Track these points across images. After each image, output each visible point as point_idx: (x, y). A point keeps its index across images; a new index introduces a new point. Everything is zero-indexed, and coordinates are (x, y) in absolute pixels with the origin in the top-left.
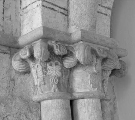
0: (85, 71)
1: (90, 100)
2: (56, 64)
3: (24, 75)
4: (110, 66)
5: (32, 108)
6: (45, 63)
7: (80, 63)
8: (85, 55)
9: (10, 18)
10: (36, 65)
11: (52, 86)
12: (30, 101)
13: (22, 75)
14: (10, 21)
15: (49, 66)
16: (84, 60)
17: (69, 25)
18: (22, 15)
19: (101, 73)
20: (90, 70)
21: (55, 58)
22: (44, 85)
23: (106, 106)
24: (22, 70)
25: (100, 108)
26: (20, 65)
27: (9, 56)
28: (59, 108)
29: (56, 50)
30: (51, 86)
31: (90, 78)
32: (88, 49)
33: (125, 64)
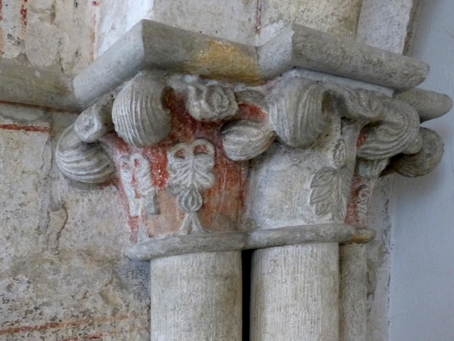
0: (297, 165)
1: (305, 248)
2: (197, 152)
3: (102, 189)
4: (384, 145)
5: (127, 277)
6: (160, 149)
7: (283, 143)
8: (300, 116)
9: (53, 15)
10: (132, 158)
11: (182, 218)
12: (119, 260)
13: (93, 191)
14: (52, 23)
16: (295, 133)
17: (260, 23)
18: (98, 5)
19: (353, 171)
20: (314, 163)
21: (197, 131)
22: (155, 216)
23: (358, 257)
24: (88, 177)
25: (334, 267)
26: (77, 162)
27: (45, 137)
28: (202, 276)
29: (195, 103)
30: (178, 218)
31: (311, 187)
32: (312, 94)
33: (438, 136)
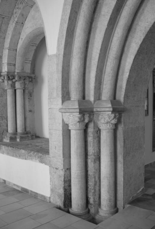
15: (9, 81)
